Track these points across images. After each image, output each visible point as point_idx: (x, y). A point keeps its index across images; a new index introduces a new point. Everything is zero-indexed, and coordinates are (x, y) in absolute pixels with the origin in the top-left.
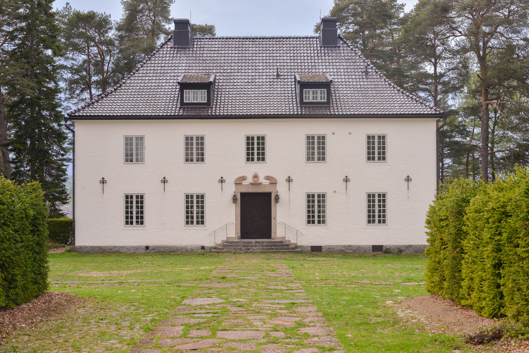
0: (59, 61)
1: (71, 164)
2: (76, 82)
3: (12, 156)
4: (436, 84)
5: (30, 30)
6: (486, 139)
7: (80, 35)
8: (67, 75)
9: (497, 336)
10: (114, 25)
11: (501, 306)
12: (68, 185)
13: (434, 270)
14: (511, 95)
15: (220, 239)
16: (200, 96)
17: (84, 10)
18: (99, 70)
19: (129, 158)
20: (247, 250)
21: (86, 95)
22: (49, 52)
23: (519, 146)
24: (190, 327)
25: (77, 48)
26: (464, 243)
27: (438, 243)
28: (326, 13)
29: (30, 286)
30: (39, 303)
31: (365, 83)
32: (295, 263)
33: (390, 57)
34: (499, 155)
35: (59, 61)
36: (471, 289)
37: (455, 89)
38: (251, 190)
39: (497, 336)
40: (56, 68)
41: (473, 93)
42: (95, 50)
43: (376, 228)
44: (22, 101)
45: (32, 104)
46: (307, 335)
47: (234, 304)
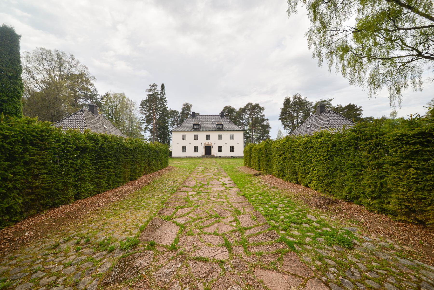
0: (169, 120)
1: (171, 140)
2: (172, 124)
3: (159, 139)
4: (243, 125)
5: (163, 113)
6: (253, 135)
7: (173, 115)
8: (170, 122)
9: (260, 174)
10: (180, 113)
11: (260, 168)
12: (171, 145)
13: (245, 161)
14: (258, 127)
15: (201, 155)
16: (197, 127)
17: (174, 110)
18: (177, 122)
19: (183, 139)
20: (207, 157)
21: (174, 127)
22: (167, 118)
23: (259, 136)
24: (198, 173)
25: (172, 117)
26: (252, 156)
27: (246, 156)
28: (222, 111)
29: (165, 165)
30: (167, 168)
31: (229, 124)
32: (216, 160)
33: (234, 119)
34: (255, 138)
35: (169, 120)
36: (253, 165)
37: (247, 125)
38: (207, 145)
39: (260, 174)
40: (168, 121)
41: (250, 126)
42: (176, 118)
43: (232, 153)
44: (161, 128)
45: (163, 128)
46: (222, 174)
47: (206, 168)
